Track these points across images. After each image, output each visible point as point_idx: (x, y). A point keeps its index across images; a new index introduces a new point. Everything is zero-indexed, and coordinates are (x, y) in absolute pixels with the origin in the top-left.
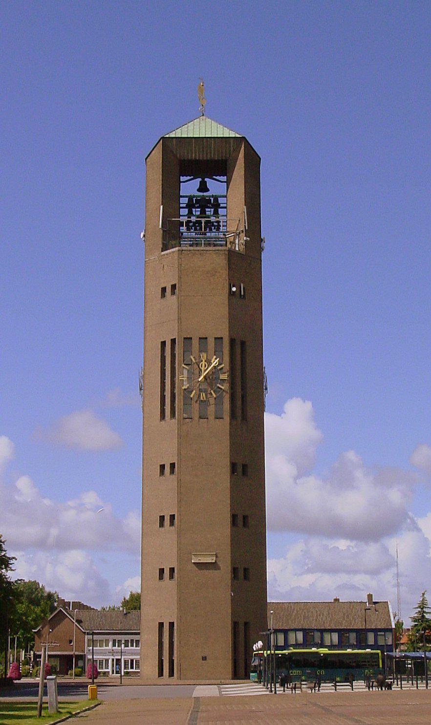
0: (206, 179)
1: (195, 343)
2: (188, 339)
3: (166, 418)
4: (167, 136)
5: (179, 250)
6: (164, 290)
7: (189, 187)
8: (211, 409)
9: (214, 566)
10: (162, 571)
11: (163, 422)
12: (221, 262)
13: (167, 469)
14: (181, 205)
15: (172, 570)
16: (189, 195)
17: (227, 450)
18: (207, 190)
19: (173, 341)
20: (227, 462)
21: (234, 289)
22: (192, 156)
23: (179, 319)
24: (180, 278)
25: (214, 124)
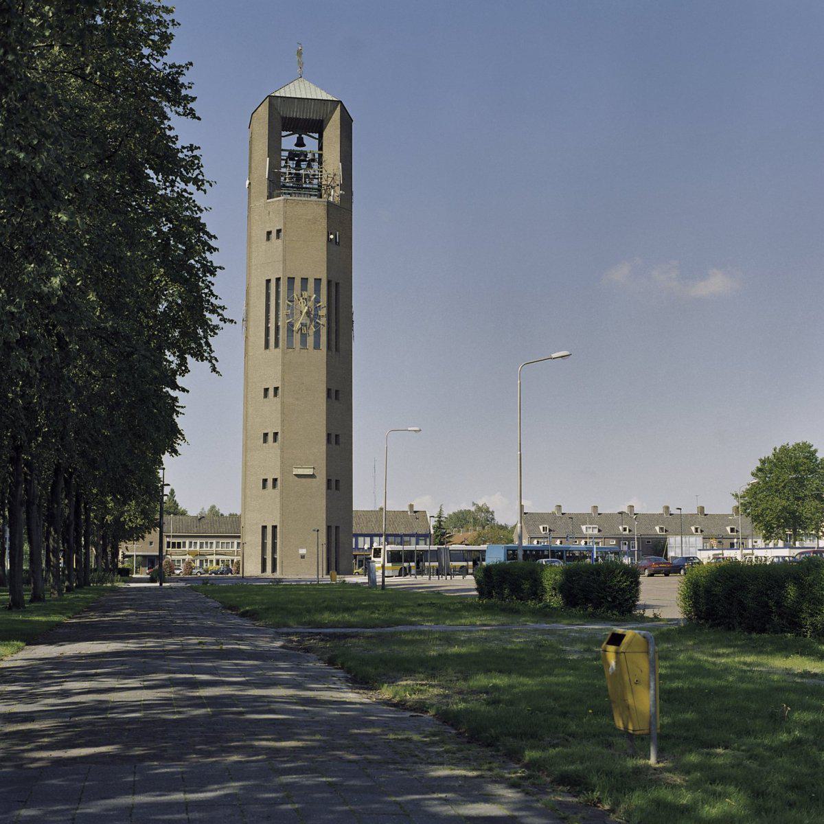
0: (303, 136)
1: (298, 283)
2: (291, 280)
3: (270, 348)
4: (273, 95)
5: (284, 199)
6: (269, 233)
7: (289, 142)
8: (310, 340)
9: (312, 476)
10: (265, 481)
11: (267, 351)
12: (321, 212)
13: (271, 392)
14: (282, 158)
15: (275, 480)
16: (289, 149)
17: (324, 378)
18: (304, 145)
19: (278, 280)
20: (323, 388)
21: (332, 237)
22: (306, 115)
23: (284, 260)
24: (285, 224)
25: (313, 87)
